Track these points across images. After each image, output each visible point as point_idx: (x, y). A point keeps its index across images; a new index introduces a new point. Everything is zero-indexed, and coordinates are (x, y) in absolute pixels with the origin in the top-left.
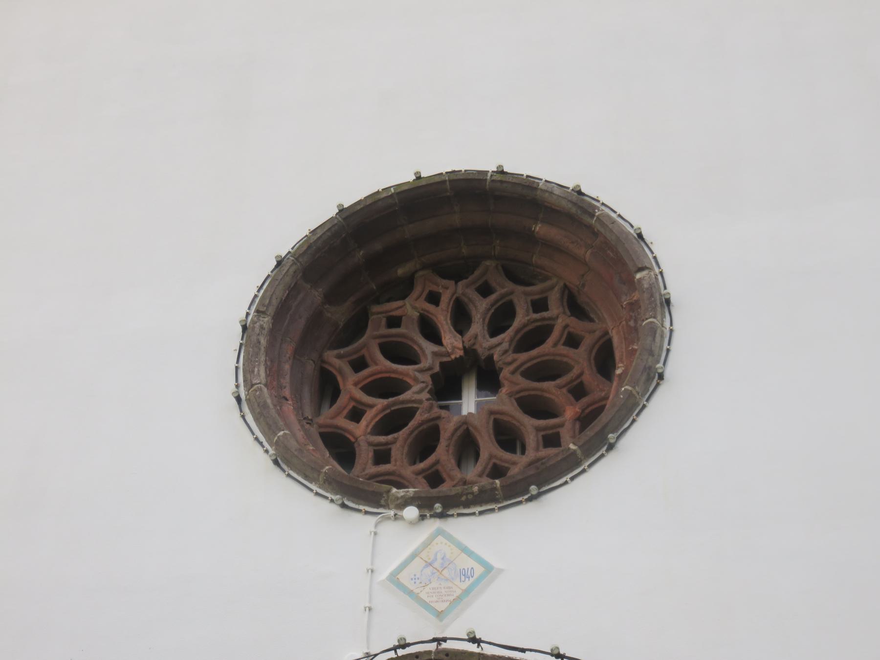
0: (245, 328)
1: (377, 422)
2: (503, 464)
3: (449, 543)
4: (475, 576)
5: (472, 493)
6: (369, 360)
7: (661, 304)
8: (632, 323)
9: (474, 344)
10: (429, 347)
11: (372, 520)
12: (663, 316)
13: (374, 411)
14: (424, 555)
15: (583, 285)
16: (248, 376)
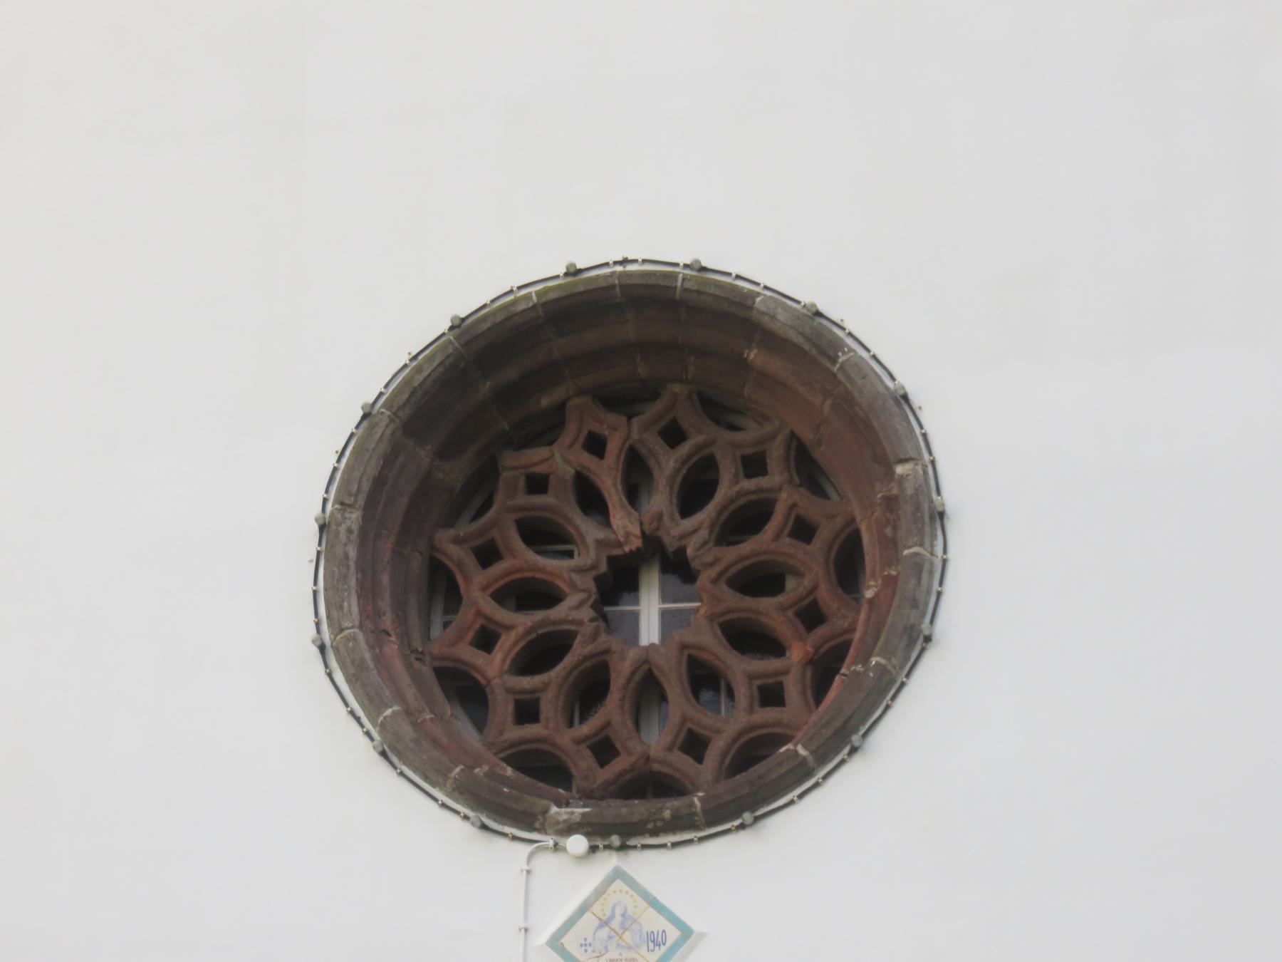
0: (322, 528)
1: (518, 654)
2: (703, 732)
3: (631, 892)
4: (669, 944)
5: (663, 820)
6: (502, 548)
7: (932, 518)
8: (888, 531)
9: (658, 529)
10: (589, 530)
11: (528, 849)
12: (934, 537)
13: (513, 635)
14: (596, 908)
15: (819, 442)
16: (334, 613)
